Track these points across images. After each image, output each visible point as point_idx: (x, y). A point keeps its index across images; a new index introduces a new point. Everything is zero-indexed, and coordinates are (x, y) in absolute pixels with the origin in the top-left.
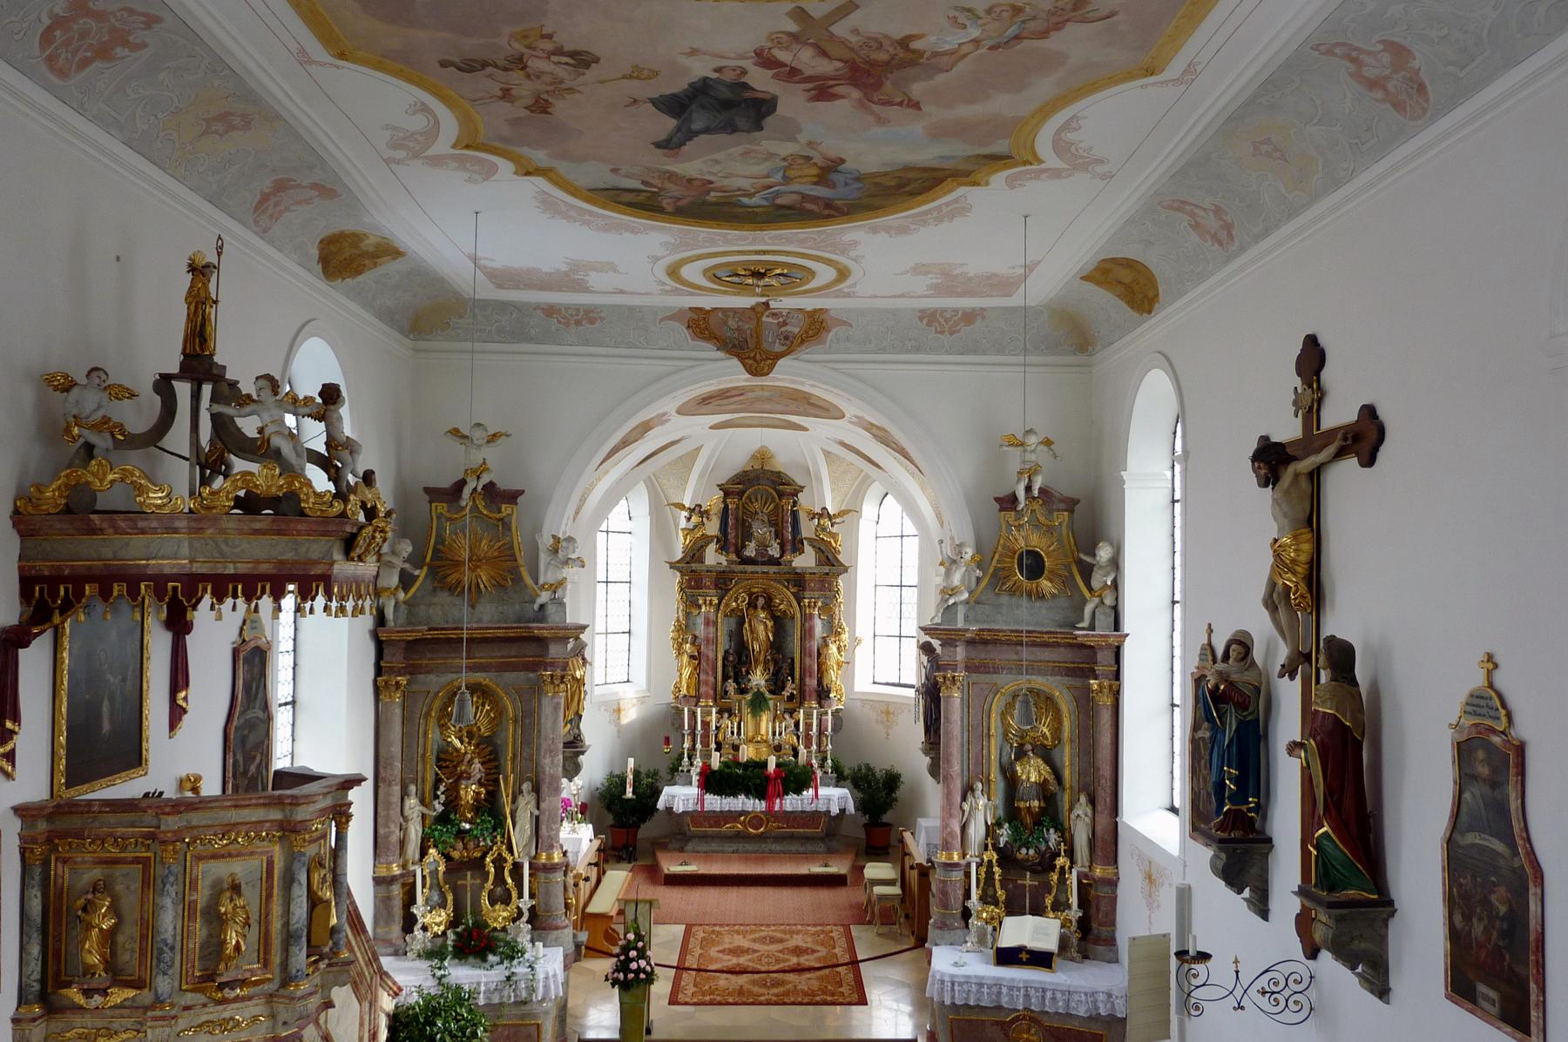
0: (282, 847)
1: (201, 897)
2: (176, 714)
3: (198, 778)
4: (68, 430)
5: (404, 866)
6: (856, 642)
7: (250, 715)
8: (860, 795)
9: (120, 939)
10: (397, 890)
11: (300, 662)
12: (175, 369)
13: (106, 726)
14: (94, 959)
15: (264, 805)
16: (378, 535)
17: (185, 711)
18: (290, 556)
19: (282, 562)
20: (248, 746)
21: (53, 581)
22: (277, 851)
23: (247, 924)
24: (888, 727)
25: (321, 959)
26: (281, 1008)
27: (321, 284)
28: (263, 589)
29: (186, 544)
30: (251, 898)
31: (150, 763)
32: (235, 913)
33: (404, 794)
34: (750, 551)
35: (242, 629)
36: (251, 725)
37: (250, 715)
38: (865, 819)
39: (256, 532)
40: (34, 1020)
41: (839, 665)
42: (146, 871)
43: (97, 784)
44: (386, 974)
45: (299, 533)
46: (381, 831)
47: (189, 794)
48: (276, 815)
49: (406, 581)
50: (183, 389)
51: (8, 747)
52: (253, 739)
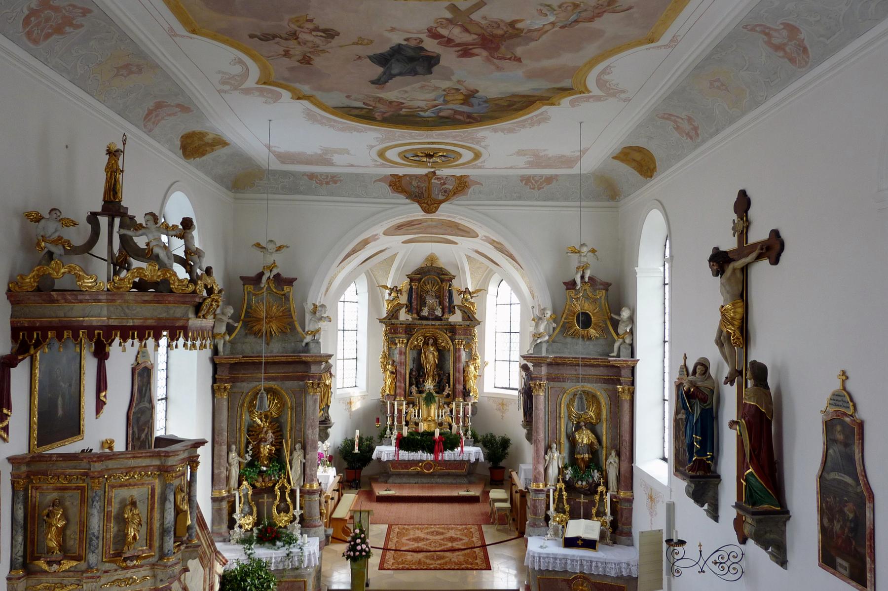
0: (160, 481)
1: (114, 509)
2: (100, 405)
3: (112, 442)
4: (38, 244)
5: (229, 491)
6: (485, 364)
7: (142, 405)
8: (487, 451)
9: (68, 532)
10: (225, 505)
11: (170, 375)
12: (99, 209)
13: (60, 412)
14: (53, 544)
15: (150, 456)
16: (214, 303)
17: (105, 403)
18: (164, 315)
19: (159, 319)
20: (141, 423)
21: (30, 330)
22: (157, 483)
23: (140, 524)
24: (503, 412)
25: (182, 544)
26: (159, 572)
27: (182, 161)
28: (149, 334)
29: (105, 309)
30: (142, 509)
31: (85, 433)
32: (133, 518)
33: (229, 450)
34: (425, 312)
35: (137, 357)
36: (142, 411)
37: (142, 405)
38: (490, 465)
39: (145, 302)
40: (19, 578)
41: (475, 377)
42: (82, 494)
43: (55, 444)
44: (219, 552)
45: (169, 302)
46: (216, 471)
47: (107, 450)
48: (156, 462)
49: (230, 329)
50: (104, 221)
51: (5, 424)
52: (143, 419)
